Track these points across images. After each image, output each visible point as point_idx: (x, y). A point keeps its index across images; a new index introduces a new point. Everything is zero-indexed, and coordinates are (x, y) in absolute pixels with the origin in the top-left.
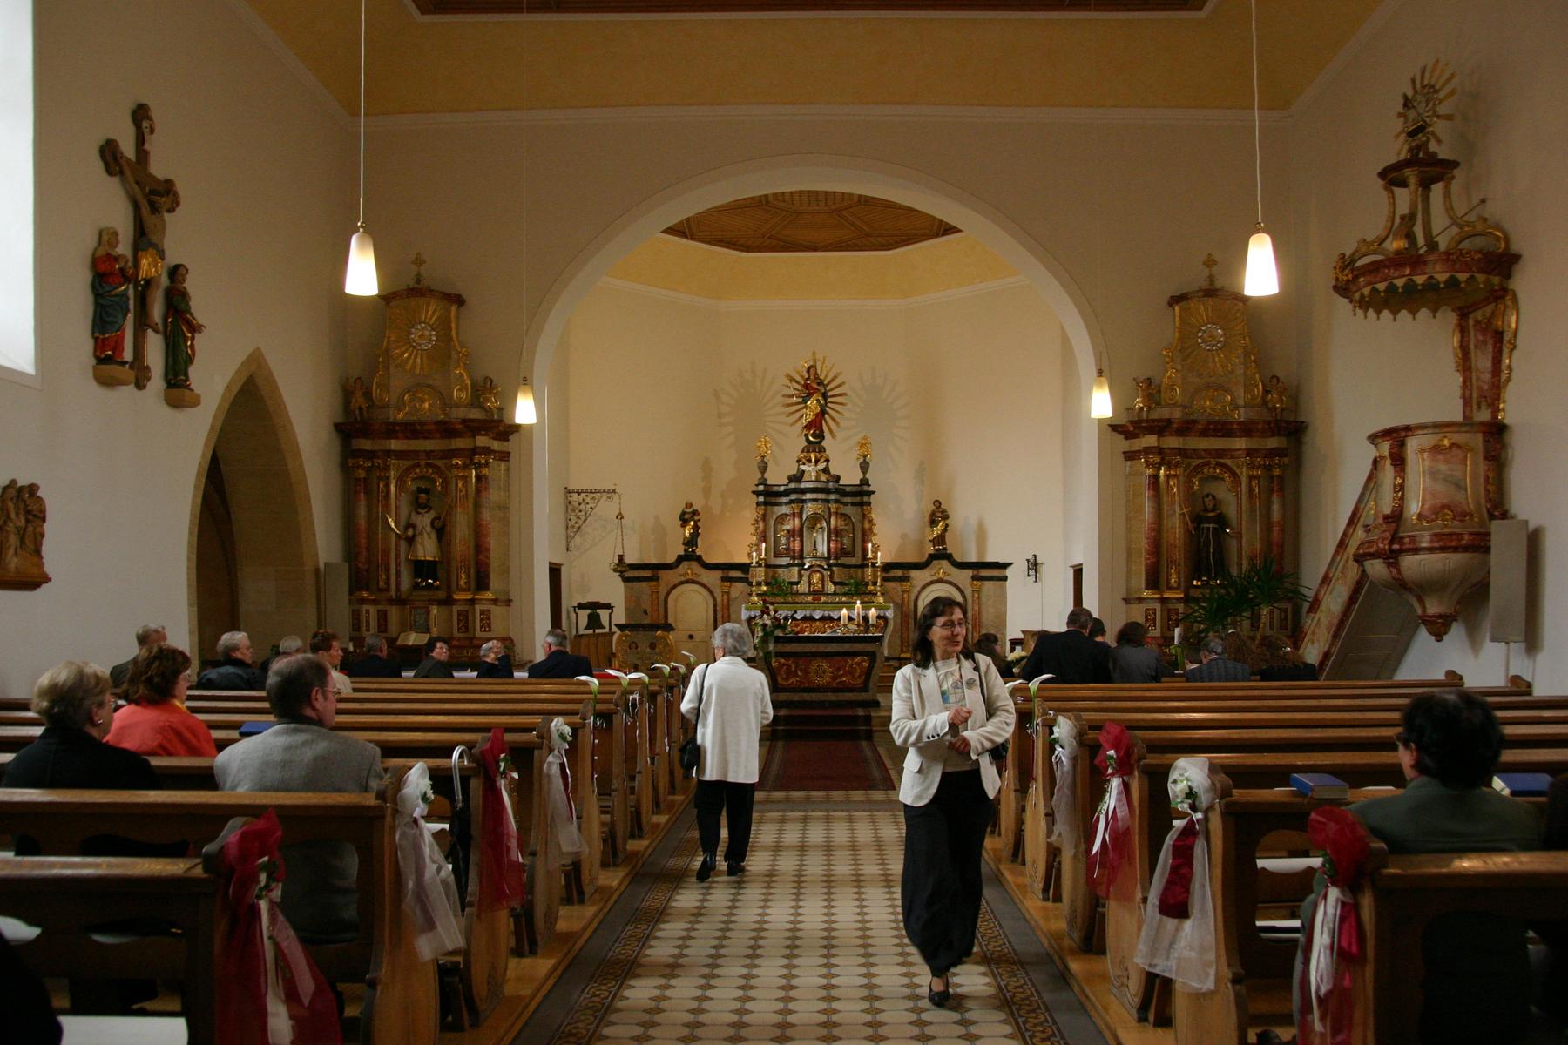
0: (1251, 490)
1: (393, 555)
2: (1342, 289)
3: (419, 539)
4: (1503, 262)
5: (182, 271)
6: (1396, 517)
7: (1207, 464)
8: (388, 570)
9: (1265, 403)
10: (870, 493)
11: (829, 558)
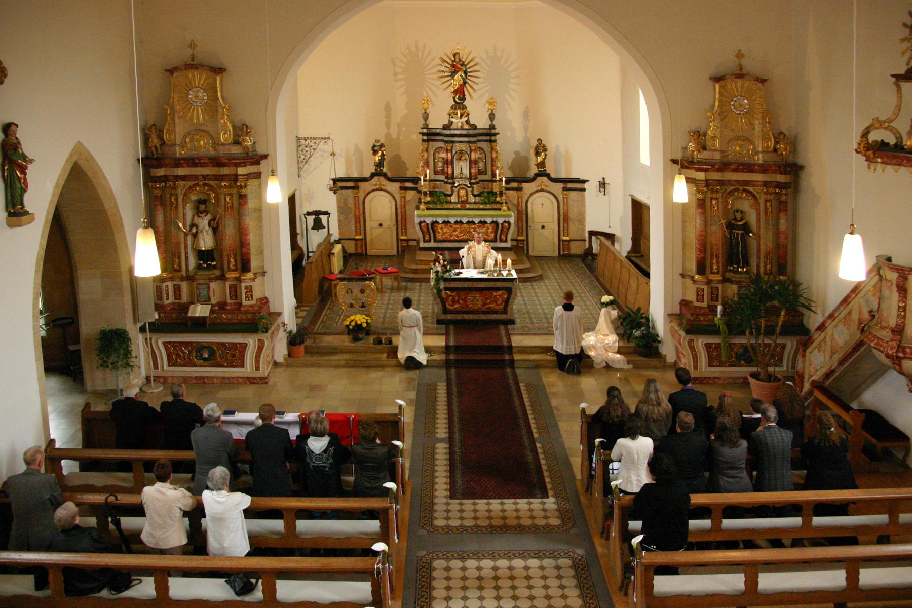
0: (766, 209)
1: (183, 246)
3: (200, 235)
5: (13, 127)
8: (179, 258)
10: (495, 135)
11: (471, 178)
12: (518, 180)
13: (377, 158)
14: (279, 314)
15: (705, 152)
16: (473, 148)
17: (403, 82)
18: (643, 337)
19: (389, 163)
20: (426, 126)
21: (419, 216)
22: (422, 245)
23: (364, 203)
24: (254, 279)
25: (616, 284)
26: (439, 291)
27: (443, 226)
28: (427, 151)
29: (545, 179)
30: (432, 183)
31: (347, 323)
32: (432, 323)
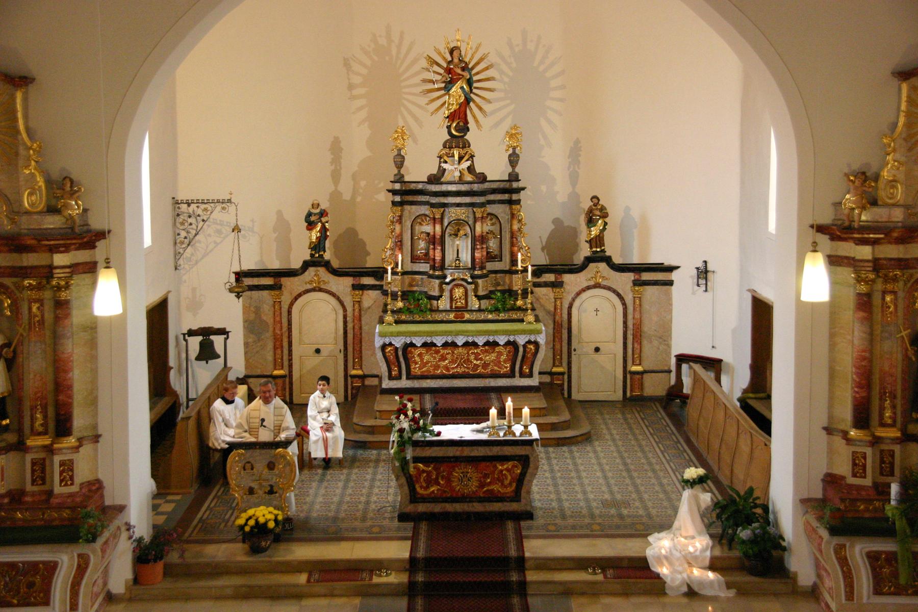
10: (519, 190)
11: (473, 268)
12: (556, 269)
13: (315, 235)
14: (121, 509)
15: (875, 210)
16: (479, 215)
17: (363, 102)
18: (754, 541)
19: (336, 244)
20: (399, 179)
21: (382, 335)
22: (387, 384)
23: (289, 312)
24: (76, 449)
25: (717, 446)
26: (404, 463)
27: (423, 351)
28: (400, 220)
29: (603, 266)
30: (407, 278)
31: (241, 521)
32: (392, 518)
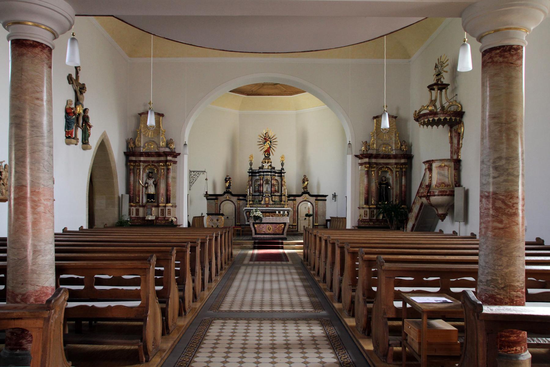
0: (396, 175)
2: (417, 120)
3: (149, 187)
4: (460, 114)
6: (429, 186)
7: (383, 167)
8: (139, 197)
9: (401, 149)
20: (251, 169)
23: (220, 206)
29: (307, 195)
